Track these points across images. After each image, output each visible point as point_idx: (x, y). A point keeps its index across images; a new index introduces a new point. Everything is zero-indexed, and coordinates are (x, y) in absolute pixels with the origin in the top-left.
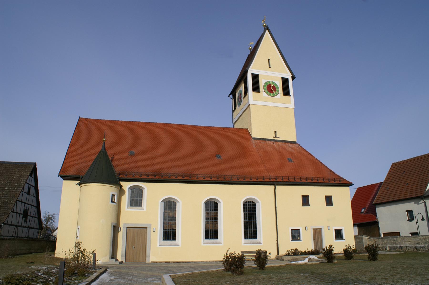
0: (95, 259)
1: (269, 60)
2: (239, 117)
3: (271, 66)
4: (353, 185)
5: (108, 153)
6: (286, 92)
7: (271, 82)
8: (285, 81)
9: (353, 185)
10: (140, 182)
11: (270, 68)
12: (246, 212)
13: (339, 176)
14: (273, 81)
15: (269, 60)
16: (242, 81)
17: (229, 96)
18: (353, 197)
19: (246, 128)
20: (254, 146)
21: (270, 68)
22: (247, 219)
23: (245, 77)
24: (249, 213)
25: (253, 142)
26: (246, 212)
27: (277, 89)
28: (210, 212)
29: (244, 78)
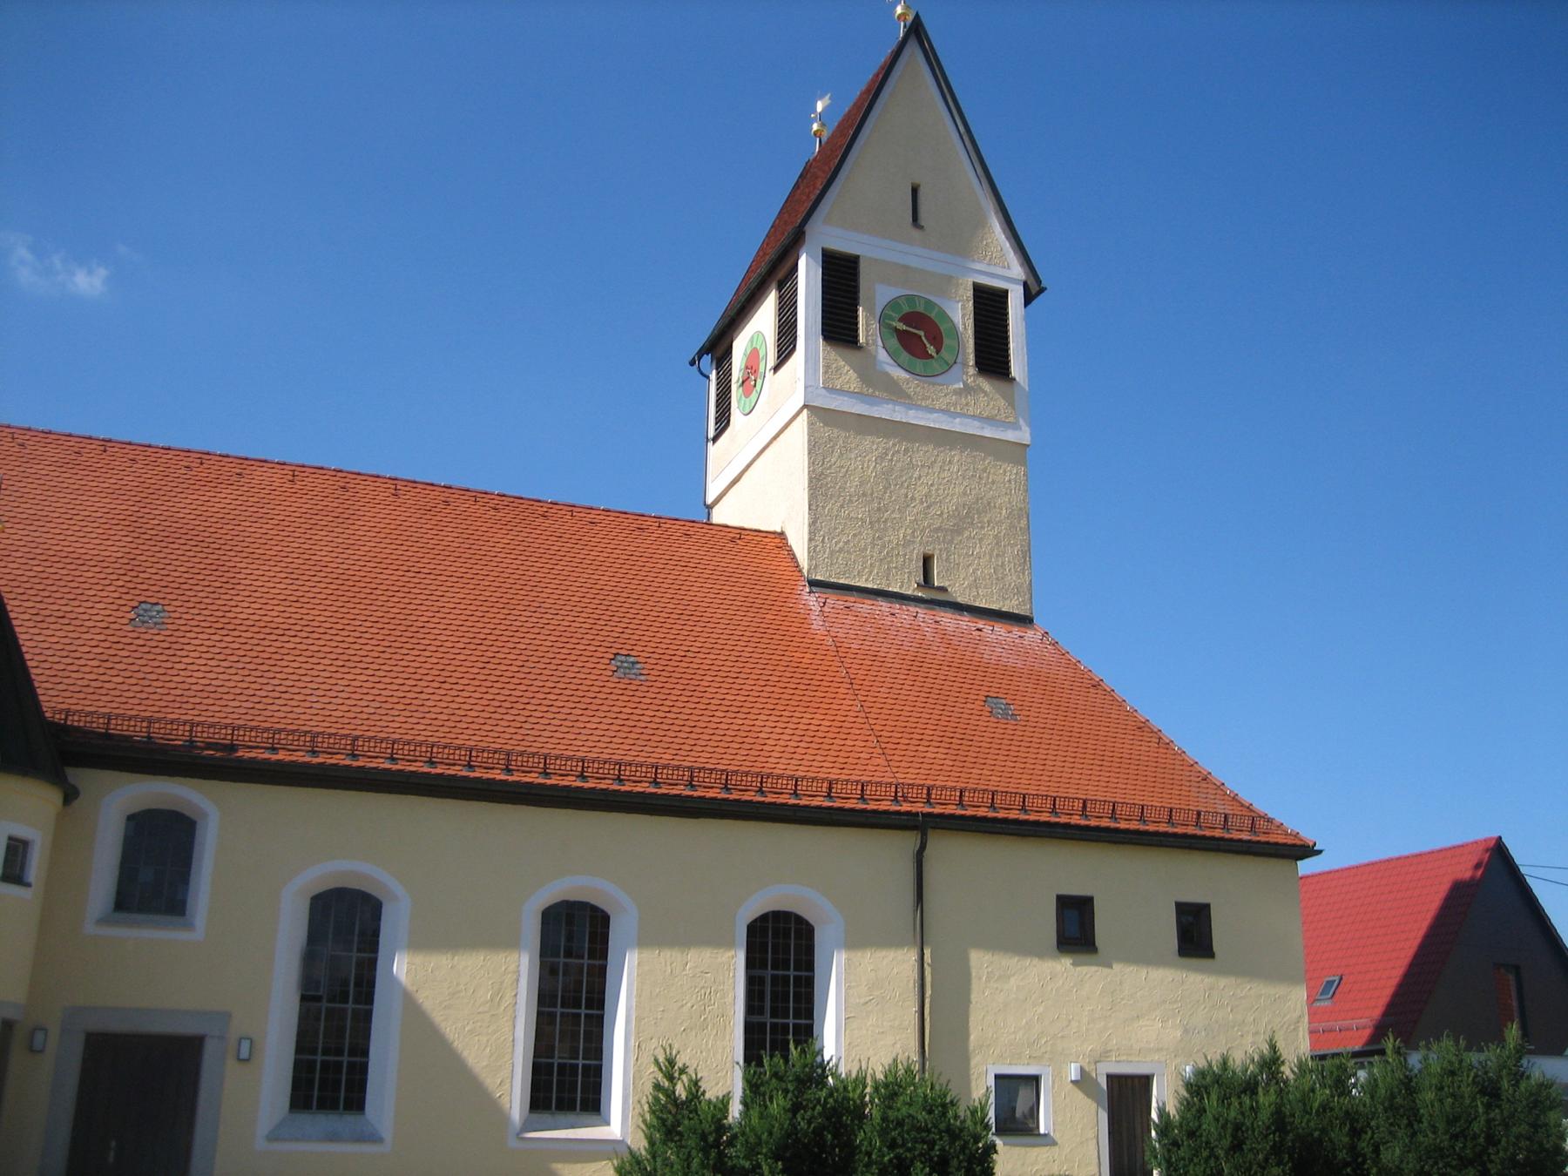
0: (1015, 279)
1: (915, 191)
2: (732, 486)
3: (922, 222)
4: (1320, 852)
5: (11, 602)
6: (992, 359)
7: (922, 302)
8: (990, 305)
9: (1320, 852)
10: (235, 781)
11: (921, 227)
12: (757, 972)
13: (1249, 808)
14: (932, 298)
15: (915, 191)
16: (771, 283)
17: (692, 363)
18: (116, 774)
19: (779, 530)
20: (817, 624)
21: (921, 227)
22: (761, 1012)
23: (796, 255)
24: (774, 978)
25: (812, 600)
26: (757, 972)
27: (946, 341)
28: (566, 964)
29: (781, 274)
